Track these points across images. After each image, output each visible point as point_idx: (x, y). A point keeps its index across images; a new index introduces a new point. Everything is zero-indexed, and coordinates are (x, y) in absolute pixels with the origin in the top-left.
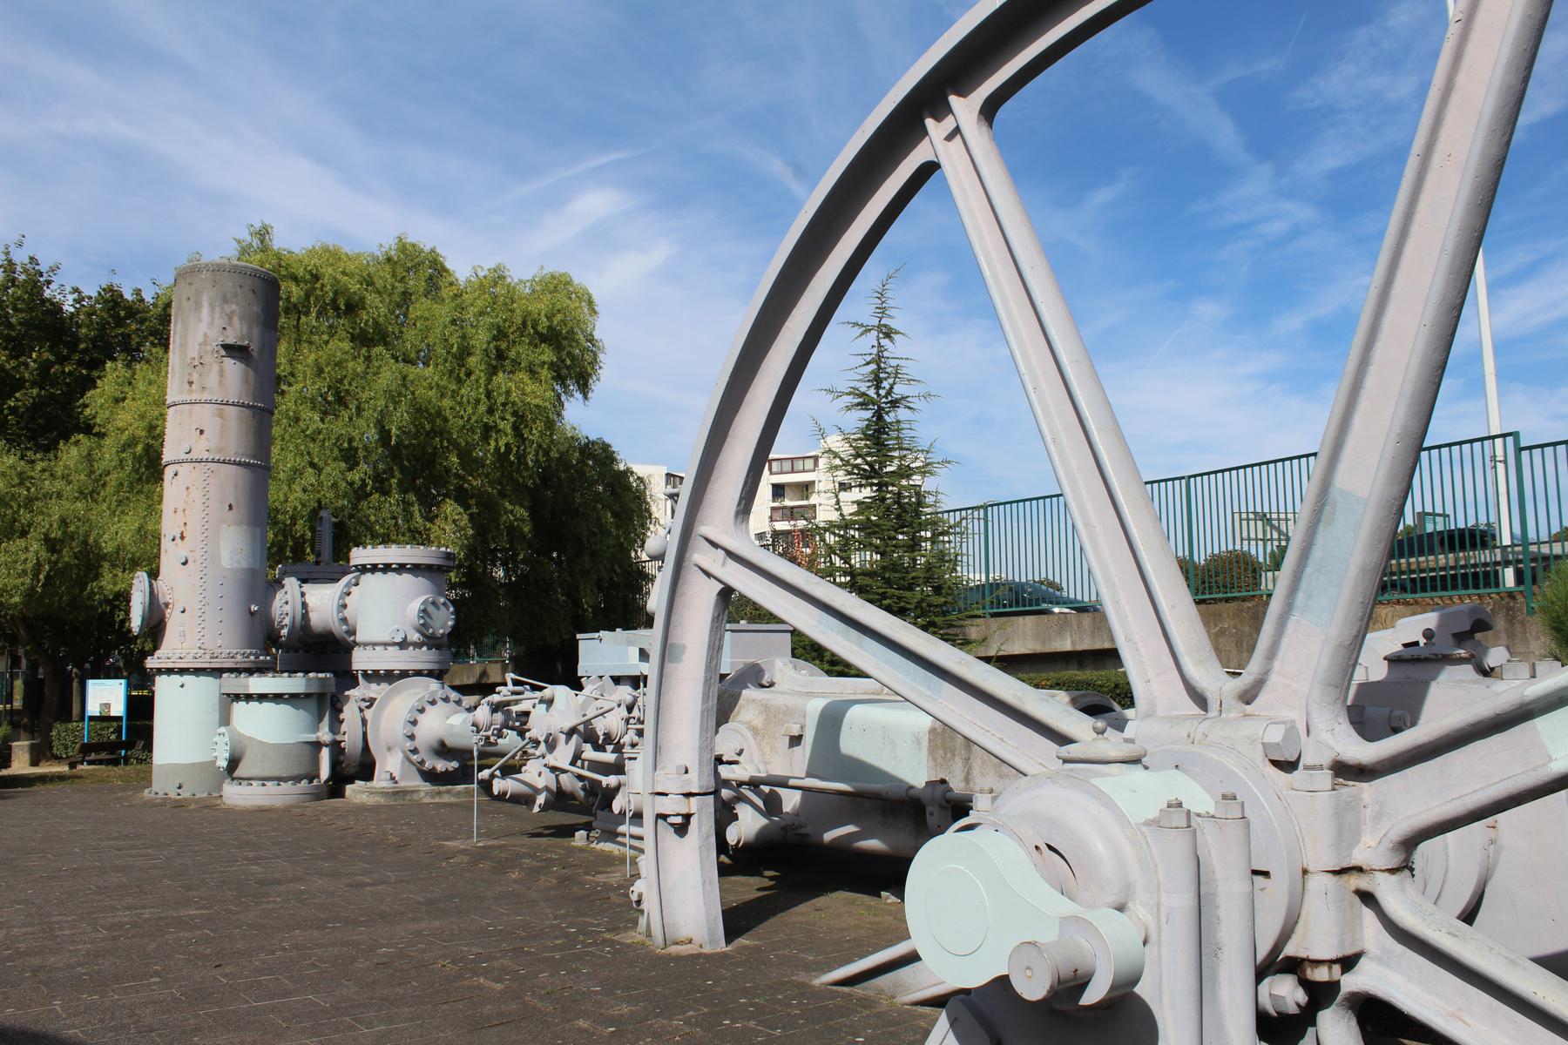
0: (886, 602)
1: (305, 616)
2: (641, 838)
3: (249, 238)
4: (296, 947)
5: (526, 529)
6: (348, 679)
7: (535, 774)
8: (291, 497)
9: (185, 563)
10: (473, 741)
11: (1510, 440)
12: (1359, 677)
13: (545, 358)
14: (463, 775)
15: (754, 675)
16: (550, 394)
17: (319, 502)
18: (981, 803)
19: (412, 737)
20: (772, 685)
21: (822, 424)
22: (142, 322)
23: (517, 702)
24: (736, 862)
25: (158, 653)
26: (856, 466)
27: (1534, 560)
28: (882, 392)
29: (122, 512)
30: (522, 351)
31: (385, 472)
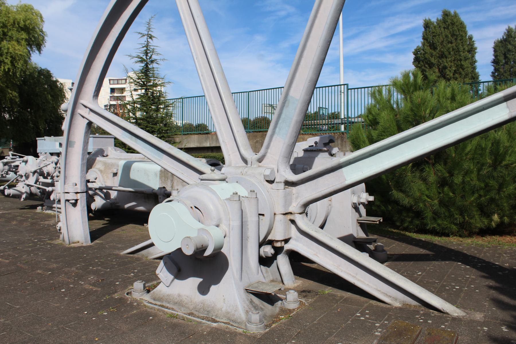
0: (147, 129)
2: (60, 208)
5: (17, 100)
7: (21, 187)
11: (346, 86)
12: (295, 155)
13: (23, 37)
15: (101, 153)
16: (25, 50)
18: (174, 193)
20: (107, 156)
21: (125, 65)
23: (14, 162)
24: (93, 215)
26: (138, 82)
27: (350, 123)
28: (148, 57)
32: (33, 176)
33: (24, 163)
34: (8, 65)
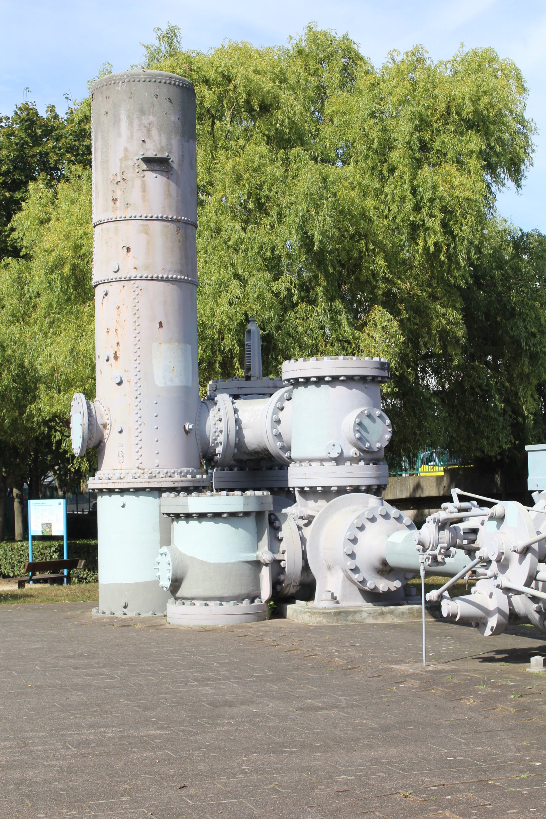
1: (239, 433)
3: (157, 43)
4: (255, 771)
6: (285, 495)
8: (219, 311)
9: (120, 384)
10: (419, 561)
13: (472, 146)
14: (408, 594)
17: (246, 315)
19: (352, 556)
22: (57, 140)
23: (461, 520)
25: (98, 474)
29: (54, 334)
30: (447, 140)
31: (310, 280)
32: (521, 562)
33: (494, 523)
34: (435, 233)
